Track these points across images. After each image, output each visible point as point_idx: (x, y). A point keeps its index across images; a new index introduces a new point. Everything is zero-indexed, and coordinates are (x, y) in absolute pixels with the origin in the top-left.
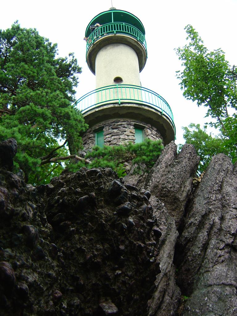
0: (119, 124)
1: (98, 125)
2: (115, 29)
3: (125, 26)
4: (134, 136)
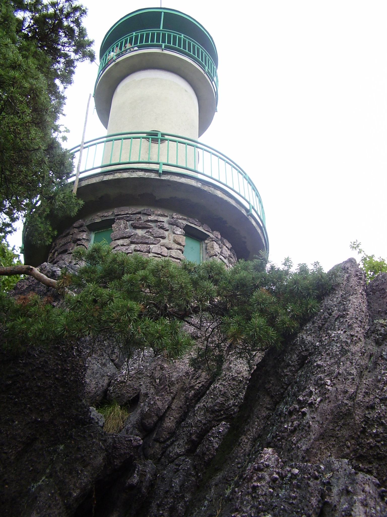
0: (150, 218)
1: (101, 215)
2: (164, 41)
3: (185, 41)
4: (182, 253)
